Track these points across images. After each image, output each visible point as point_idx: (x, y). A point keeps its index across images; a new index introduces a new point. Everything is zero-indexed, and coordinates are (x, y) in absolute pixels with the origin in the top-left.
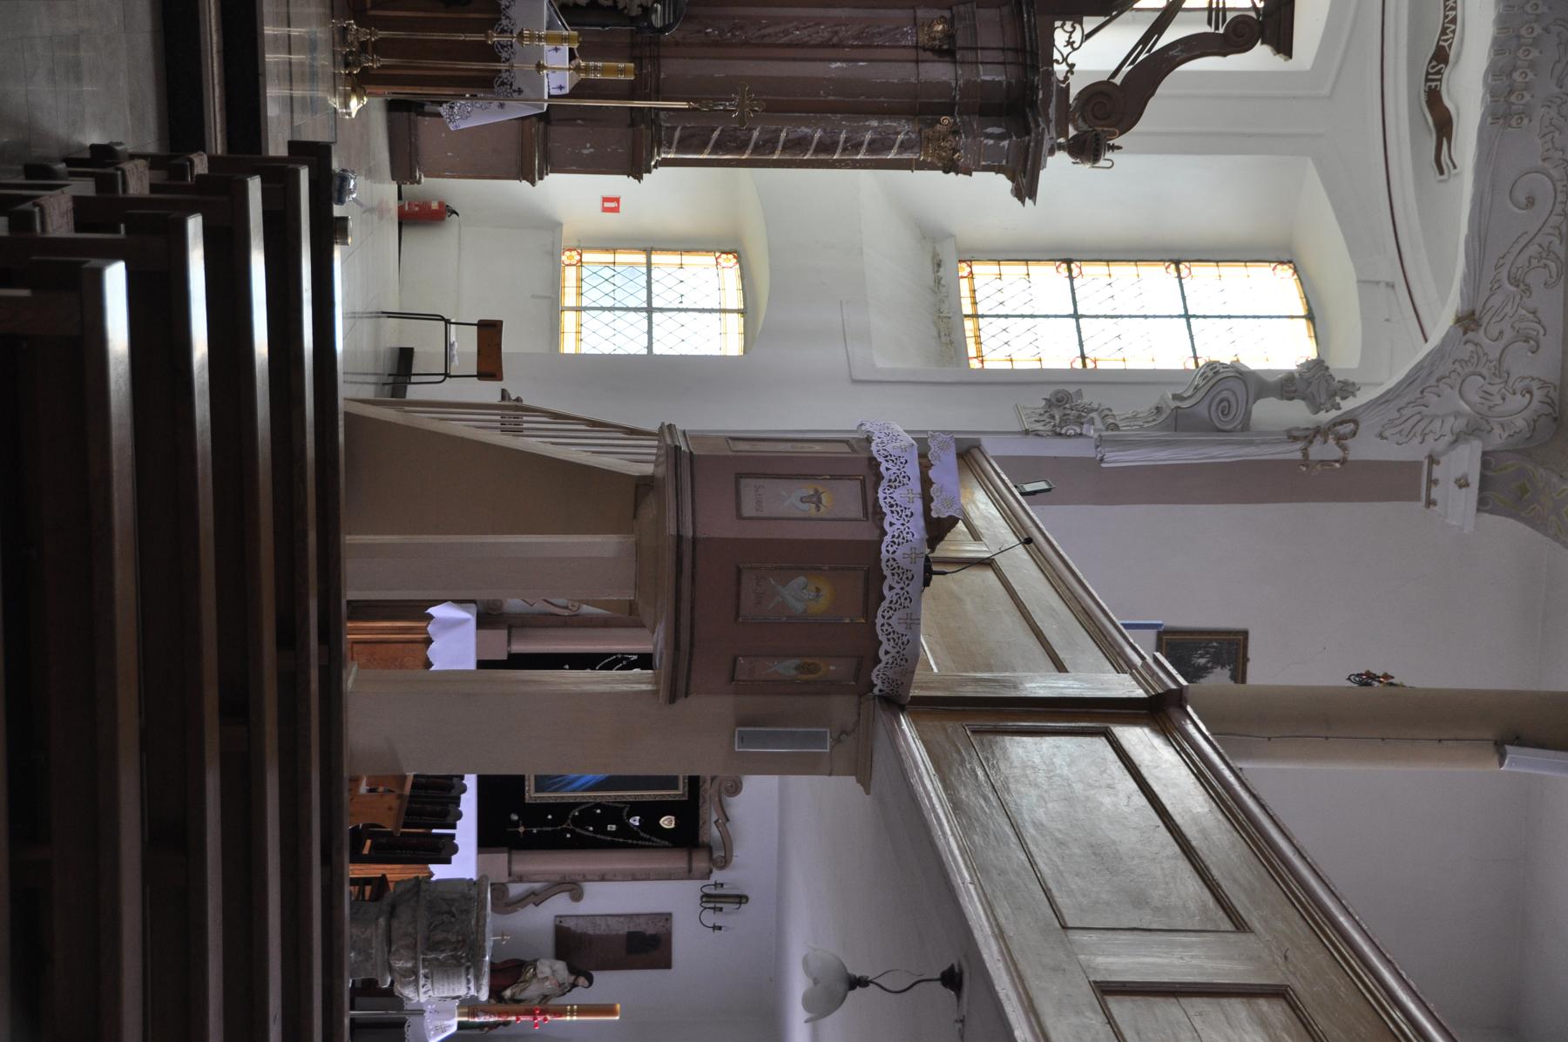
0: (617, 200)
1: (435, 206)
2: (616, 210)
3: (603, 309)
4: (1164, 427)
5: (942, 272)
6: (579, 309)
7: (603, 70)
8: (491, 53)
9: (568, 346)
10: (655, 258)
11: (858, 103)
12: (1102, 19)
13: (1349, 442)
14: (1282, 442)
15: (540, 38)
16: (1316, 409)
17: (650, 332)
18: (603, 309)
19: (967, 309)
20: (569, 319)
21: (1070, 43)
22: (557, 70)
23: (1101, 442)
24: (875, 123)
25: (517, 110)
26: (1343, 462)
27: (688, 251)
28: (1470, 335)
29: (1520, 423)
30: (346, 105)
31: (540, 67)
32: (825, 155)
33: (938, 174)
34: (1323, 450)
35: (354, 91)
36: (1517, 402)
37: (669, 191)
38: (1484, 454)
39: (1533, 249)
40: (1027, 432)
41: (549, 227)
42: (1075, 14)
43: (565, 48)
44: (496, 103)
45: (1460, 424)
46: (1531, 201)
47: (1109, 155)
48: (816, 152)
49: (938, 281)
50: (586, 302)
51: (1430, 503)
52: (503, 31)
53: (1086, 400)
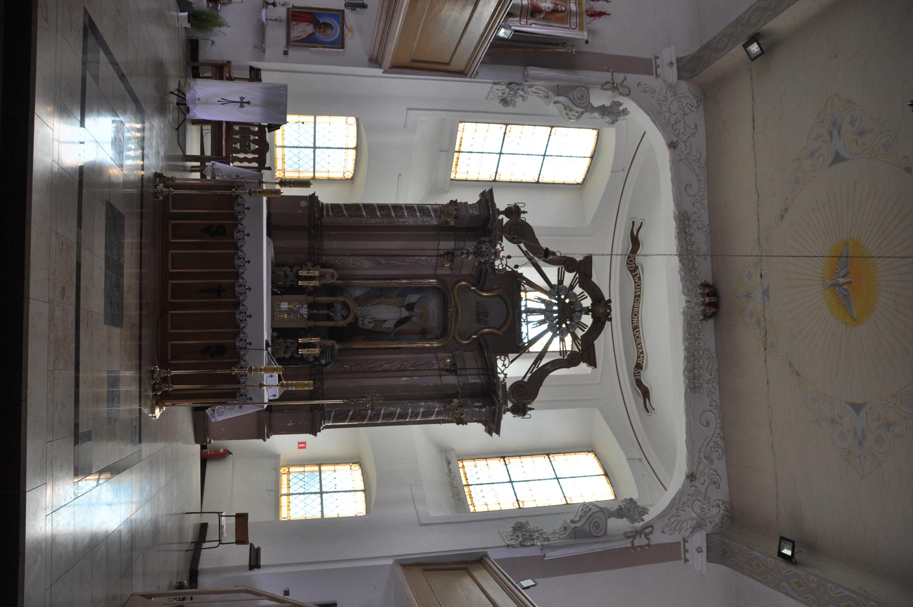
0: (305, 443)
1: (222, 451)
2: (304, 447)
3: (300, 494)
4: (569, 537)
5: (451, 466)
6: (288, 495)
7: (295, 385)
8: (235, 379)
9: (284, 514)
10: (323, 468)
11: (414, 395)
12: (516, 355)
13: (650, 536)
14: (622, 540)
15: (261, 370)
16: (633, 521)
17: (322, 504)
18: (300, 494)
19: (464, 483)
20: (284, 500)
21: (504, 365)
22: (271, 388)
23: (543, 547)
24: (423, 404)
25: (249, 410)
26: (649, 545)
27: (338, 464)
28: (693, 483)
29: (717, 520)
30: (153, 412)
31: (261, 385)
32: (402, 419)
33: (454, 425)
34: (641, 541)
35: (157, 404)
36: (714, 511)
37: (329, 439)
38: (707, 535)
39: (712, 444)
40: (508, 546)
41: (274, 457)
42: (505, 353)
43: (276, 375)
44: (237, 406)
45: (694, 523)
46: (708, 424)
47: (529, 412)
48: (398, 418)
49: (450, 470)
50: (291, 491)
51: (686, 560)
52: (242, 368)
53: (532, 526)
